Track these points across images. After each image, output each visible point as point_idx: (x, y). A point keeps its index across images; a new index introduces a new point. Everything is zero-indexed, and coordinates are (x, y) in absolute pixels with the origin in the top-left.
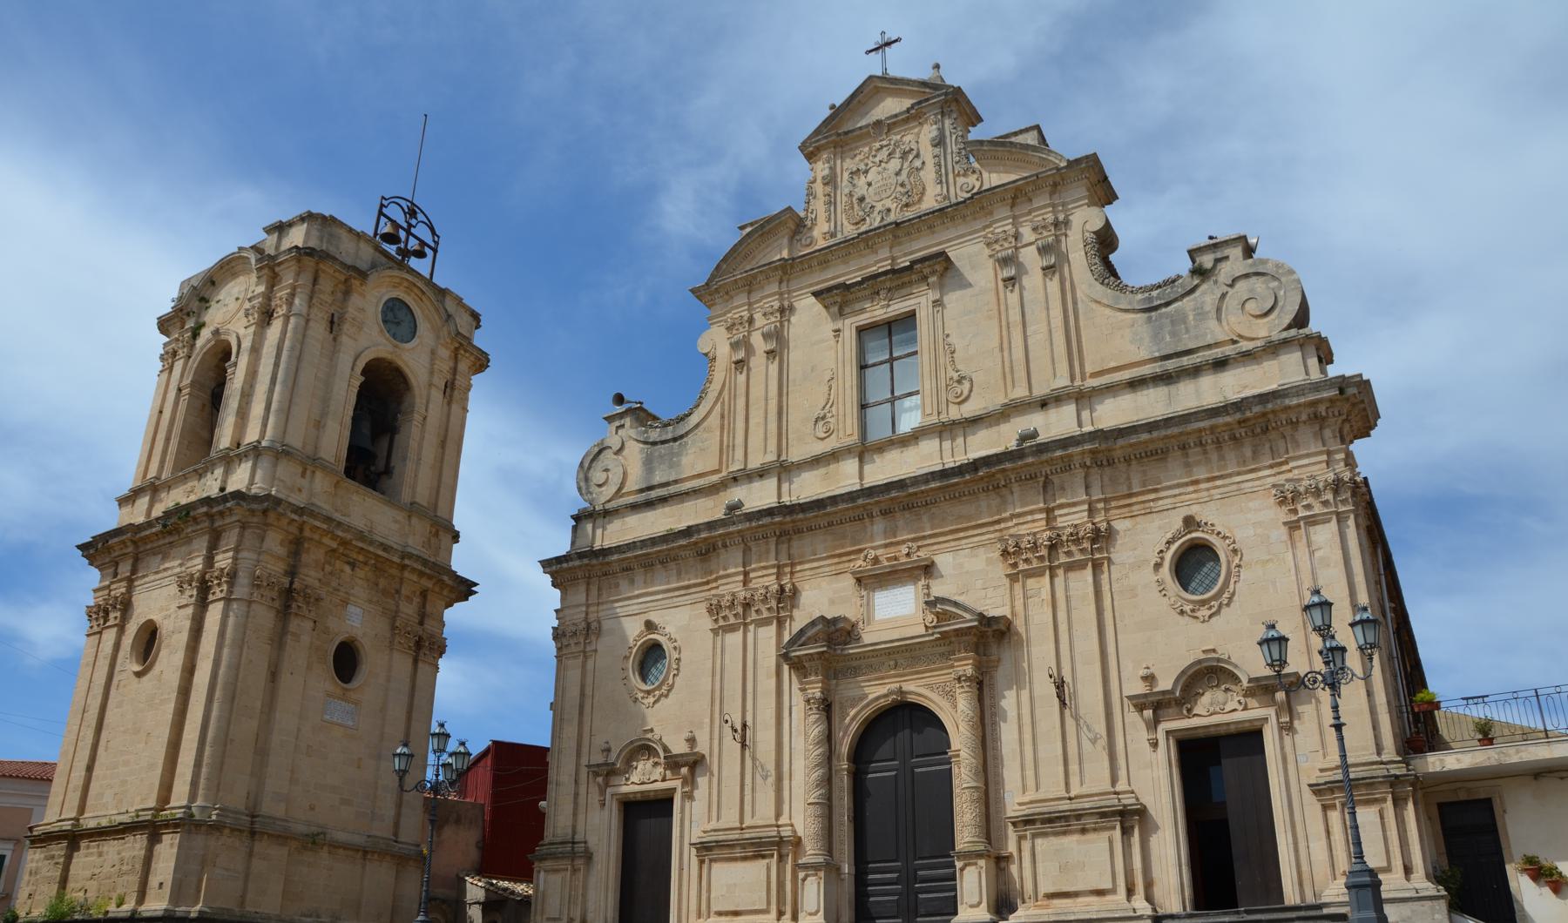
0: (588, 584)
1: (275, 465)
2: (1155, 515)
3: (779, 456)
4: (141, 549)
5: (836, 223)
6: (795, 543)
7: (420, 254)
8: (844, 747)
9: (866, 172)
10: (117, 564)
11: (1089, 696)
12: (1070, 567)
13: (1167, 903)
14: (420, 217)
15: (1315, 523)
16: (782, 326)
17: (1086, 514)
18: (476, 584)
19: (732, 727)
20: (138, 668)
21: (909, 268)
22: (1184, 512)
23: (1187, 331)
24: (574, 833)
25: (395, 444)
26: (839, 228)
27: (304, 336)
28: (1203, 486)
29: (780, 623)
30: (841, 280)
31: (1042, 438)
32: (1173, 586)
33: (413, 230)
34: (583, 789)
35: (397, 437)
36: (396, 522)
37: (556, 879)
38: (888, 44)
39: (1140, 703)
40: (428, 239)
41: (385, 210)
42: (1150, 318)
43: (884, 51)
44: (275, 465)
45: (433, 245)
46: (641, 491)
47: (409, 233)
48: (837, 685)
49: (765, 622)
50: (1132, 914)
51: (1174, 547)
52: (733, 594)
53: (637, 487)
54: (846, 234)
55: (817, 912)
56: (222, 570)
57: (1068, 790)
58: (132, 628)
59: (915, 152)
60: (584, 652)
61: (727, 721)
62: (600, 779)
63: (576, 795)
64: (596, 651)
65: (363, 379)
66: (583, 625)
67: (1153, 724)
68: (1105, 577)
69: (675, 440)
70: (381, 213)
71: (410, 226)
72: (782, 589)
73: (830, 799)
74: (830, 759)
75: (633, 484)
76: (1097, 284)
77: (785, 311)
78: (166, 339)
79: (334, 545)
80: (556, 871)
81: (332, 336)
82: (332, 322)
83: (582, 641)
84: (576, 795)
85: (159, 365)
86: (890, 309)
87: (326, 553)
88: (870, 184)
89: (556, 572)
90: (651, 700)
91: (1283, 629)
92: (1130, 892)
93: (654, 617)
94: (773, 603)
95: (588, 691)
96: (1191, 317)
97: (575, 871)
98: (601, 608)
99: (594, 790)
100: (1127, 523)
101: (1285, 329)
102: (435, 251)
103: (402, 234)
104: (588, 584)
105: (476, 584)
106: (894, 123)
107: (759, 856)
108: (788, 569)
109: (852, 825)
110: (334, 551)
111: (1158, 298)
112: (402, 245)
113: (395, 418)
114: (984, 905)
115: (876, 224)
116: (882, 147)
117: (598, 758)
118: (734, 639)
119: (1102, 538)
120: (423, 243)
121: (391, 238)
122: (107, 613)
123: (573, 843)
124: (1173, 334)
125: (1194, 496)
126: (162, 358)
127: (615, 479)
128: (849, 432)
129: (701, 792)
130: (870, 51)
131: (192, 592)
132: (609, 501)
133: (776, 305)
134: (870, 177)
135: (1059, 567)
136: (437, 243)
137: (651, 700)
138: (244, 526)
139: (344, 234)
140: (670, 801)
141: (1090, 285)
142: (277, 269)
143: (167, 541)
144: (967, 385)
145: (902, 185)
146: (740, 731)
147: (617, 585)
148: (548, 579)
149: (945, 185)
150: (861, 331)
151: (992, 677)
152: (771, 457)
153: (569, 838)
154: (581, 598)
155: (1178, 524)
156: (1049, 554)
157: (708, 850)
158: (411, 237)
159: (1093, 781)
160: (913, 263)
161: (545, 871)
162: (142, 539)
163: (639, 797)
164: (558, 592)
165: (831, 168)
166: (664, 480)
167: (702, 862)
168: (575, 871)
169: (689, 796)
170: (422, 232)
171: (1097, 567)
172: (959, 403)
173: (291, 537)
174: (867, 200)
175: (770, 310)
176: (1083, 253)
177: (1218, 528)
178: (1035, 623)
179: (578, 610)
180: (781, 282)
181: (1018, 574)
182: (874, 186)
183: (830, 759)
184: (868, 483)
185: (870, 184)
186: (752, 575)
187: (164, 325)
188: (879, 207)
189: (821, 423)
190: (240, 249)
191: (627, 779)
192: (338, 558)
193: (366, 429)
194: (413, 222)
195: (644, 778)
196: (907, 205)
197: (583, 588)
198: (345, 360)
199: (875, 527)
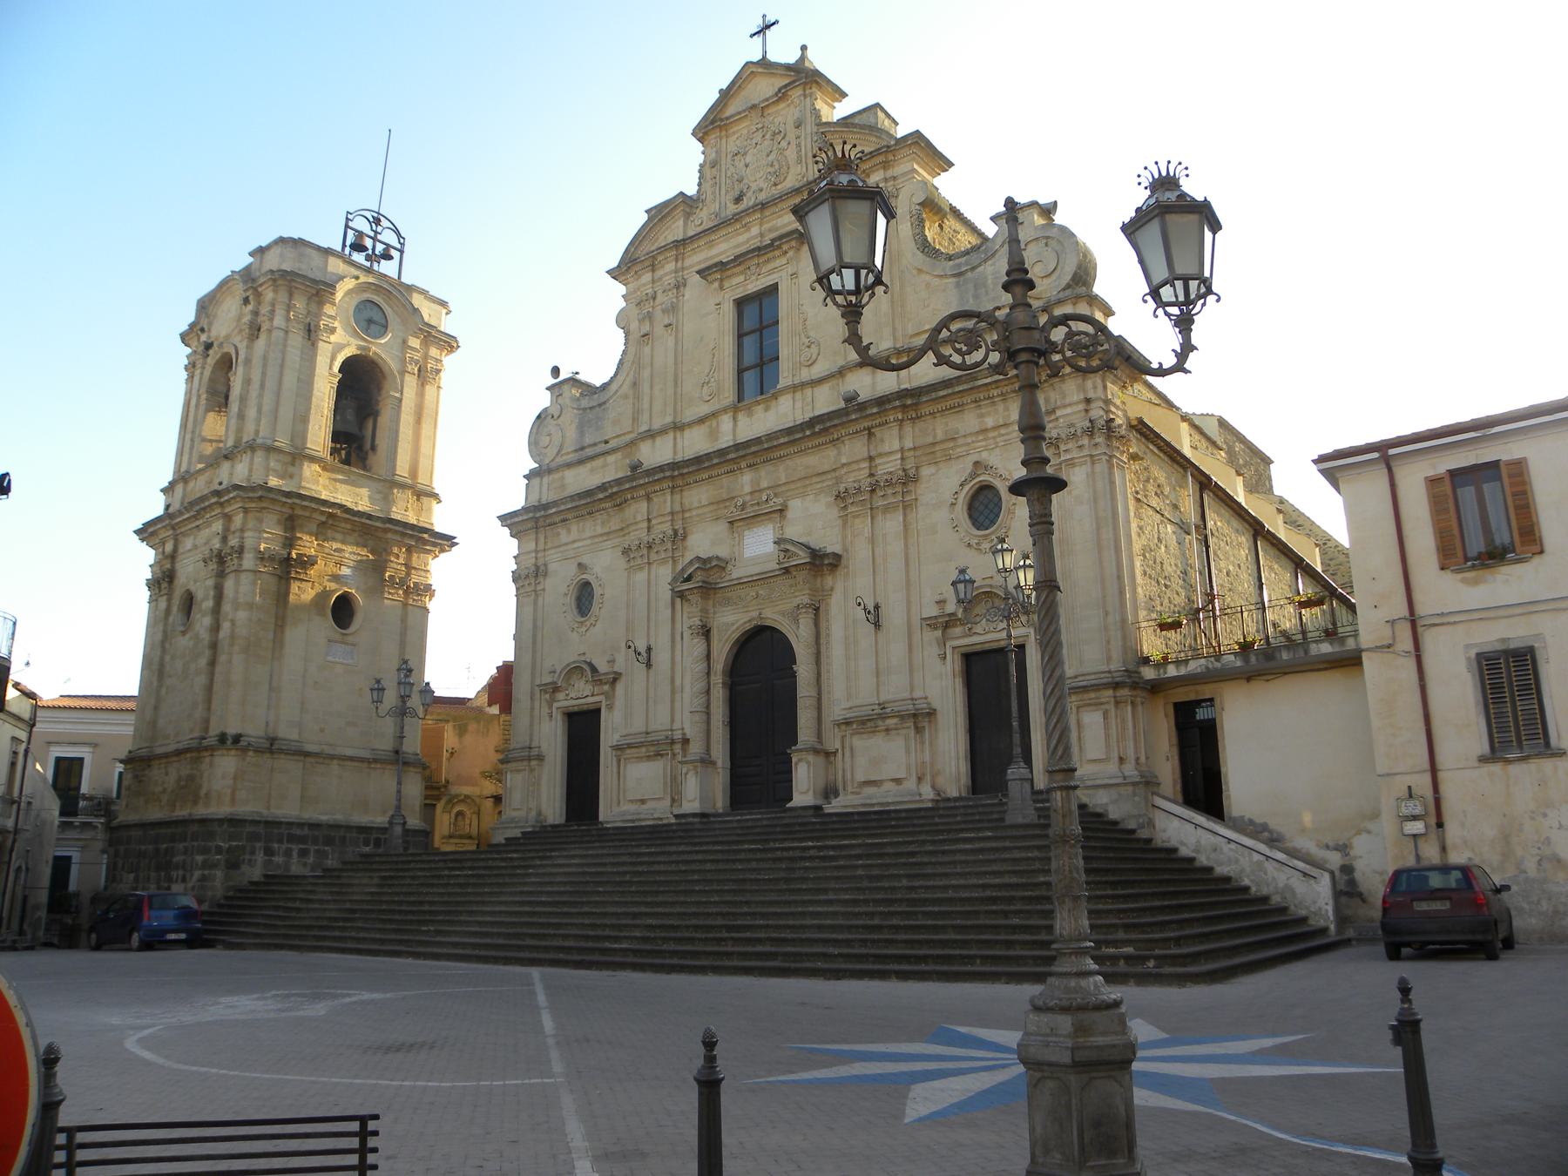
0: (537, 533)
1: (267, 459)
2: (953, 461)
3: (675, 417)
4: (178, 532)
5: (720, 203)
6: (685, 494)
7: (387, 256)
8: (719, 665)
9: (745, 154)
10: (164, 544)
11: (894, 616)
12: (887, 509)
13: (948, 790)
14: (384, 223)
15: (1074, 465)
16: (678, 301)
17: (899, 462)
18: (455, 538)
19: (865, 609)
20: (182, 629)
21: (771, 245)
22: (975, 458)
23: (987, 293)
24: (531, 740)
25: (378, 424)
26: (723, 208)
27: (285, 346)
28: (991, 434)
29: (675, 562)
30: (716, 260)
31: (860, 399)
32: (965, 522)
33: (379, 237)
34: (537, 704)
35: (379, 419)
36: (380, 492)
37: (519, 778)
38: (768, 27)
39: (931, 623)
40: (394, 241)
41: (350, 224)
42: (958, 283)
43: (765, 34)
44: (267, 459)
45: (399, 246)
46: (576, 451)
47: (374, 239)
48: (715, 613)
49: (663, 561)
50: (918, 798)
51: (967, 488)
52: (640, 539)
53: (573, 449)
54: (728, 213)
55: (808, 790)
56: (232, 547)
57: (878, 699)
58: (178, 593)
59: (782, 135)
60: (535, 591)
61: (860, 604)
62: (547, 696)
63: (532, 709)
64: (544, 590)
65: (341, 375)
66: (533, 568)
67: (943, 642)
68: (540, 599)
69: (600, 405)
70: (347, 226)
71: (376, 232)
72: (676, 532)
73: (708, 707)
74: (708, 674)
75: (570, 446)
76: (918, 252)
77: (680, 286)
78: (189, 350)
79: (324, 519)
80: (518, 771)
81: (310, 342)
82: (309, 331)
83: (533, 581)
84: (532, 709)
85: (184, 375)
86: (758, 283)
87: (318, 525)
88: (747, 166)
89: (511, 524)
90: (584, 629)
91: (384, 683)
92: (920, 779)
93: (585, 560)
94: (669, 545)
95: (539, 623)
96: (990, 281)
97: (532, 770)
98: (547, 553)
99: (544, 704)
100: (932, 469)
101: (1064, 289)
102: (401, 252)
103: (368, 243)
104: (537, 533)
105: (455, 538)
106: (767, 106)
107: (658, 755)
108: (680, 516)
109: (728, 728)
110: (323, 523)
111: (967, 263)
112: (370, 252)
113: (377, 402)
114: (811, 792)
115: (751, 203)
116: (758, 130)
117: (547, 679)
118: (641, 576)
119: (908, 479)
120: (388, 246)
121: (358, 247)
122: (159, 583)
123: (672, 730)
124: (976, 297)
125: (983, 443)
126: (186, 368)
127: (557, 439)
128: (727, 395)
129: (619, 702)
130: (754, 34)
131: (213, 566)
132: (553, 460)
133: (673, 281)
134: (749, 159)
135: (877, 508)
136: (403, 245)
137: (584, 629)
138: (246, 511)
139: (314, 253)
140: (599, 711)
141: (914, 254)
142: (260, 289)
143: (193, 525)
144: (814, 350)
145: (772, 165)
146: (645, 655)
147: (559, 534)
148: (507, 531)
149: (804, 165)
150: (740, 304)
151: (828, 604)
152: (669, 419)
153: (527, 744)
154: (532, 546)
155: (970, 467)
156: (871, 497)
157: (618, 748)
158: (765, 323)
159: (895, 690)
160: (773, 240)
161: (511, 771)
162: (177, 524)
163: (576, 709)
164: (515, 542)
165: (717, 152)
166: (592, 442)
167: (619, 761)
168: (532, 770)
169: (610, 707)
170: (389, 237)
171: (907, 507)
172: (809, 366)
173: (287, 515)
174: (745, 181)
175: (668, 287)
176: (909, 224)
177: (1001, 471)
178: (859, 555)
179: (893, 458)
180: (677, 260)
181: (1061, 464)
182: (751, 167)
183: (708, 674)
184: (742, 438)
185: (747, 166)
186: (653, 522)
187: (185, 338)
188: (754, 186)
189: (706, 387)
190: (260, 252)
191: (567, 695)
192: (330, 528)
193: (350, 415)
194: (379, 229)
195: (580, 694)
196: (775, 185)
197: (895, 431)
198: (322, 361)
199: (744, 477)
